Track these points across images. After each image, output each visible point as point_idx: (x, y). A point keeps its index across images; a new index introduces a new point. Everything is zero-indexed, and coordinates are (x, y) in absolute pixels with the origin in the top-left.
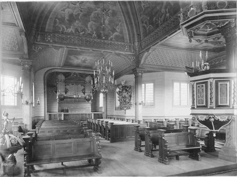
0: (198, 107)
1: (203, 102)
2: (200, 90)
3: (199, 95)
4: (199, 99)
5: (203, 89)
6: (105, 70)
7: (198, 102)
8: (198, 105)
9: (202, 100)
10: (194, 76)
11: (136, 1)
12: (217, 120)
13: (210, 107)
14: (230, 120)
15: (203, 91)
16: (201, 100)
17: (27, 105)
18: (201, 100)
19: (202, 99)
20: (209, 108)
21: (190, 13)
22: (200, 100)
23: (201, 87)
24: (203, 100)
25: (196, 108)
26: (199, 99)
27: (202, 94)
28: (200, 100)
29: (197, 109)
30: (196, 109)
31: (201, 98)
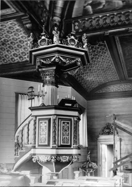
0: (39, 146)
2: (43, 127)
5: (69, 127)
6: (130, 36)
7: (63, 140)
8: (39, 144)
9: (67, 138)
10: (17, 118)
11: (33, 1)
12: (59, 160)
13: (52, 146)
14: (71, 161)
15: (68, 129)
16: (66, 138)
17: (116, 176)
18: (66, 138)
19: (68, 138)
20: (51, 147)
21: (64, 18)
22: (65, 138)
23: (66, 124)
25: (37, 147)
26: (41, 137)
28: (65, 138)
29: (59, 149)
30: (38, 148)
31: (66, 136)
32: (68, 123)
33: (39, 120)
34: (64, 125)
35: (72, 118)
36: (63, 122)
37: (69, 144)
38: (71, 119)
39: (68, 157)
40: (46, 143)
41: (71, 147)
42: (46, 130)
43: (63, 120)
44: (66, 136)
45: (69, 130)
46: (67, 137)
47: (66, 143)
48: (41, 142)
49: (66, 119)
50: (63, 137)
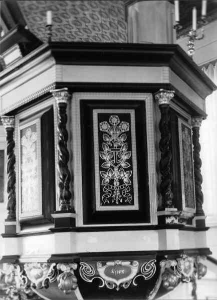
1: (132, 192)
3: (107, 158)
4: (107, 177)
5: (128, 134)
7: (102, 193)
9: (121, 181)
15: (128, 141)
16: (117, 183)
18: (117, 183)
20: (154, 222)
22: (112, 181)
23: (115, 120)
24: (132, 186)
25: (80, 223)
27: (125, 157)
28: (112, 181)
31: (116, 174)
32: (125, 118)
33: (86, 108)
34: (105, 126)
35: (147, 98)
36: (99, 115)
37: (136, 207)
38: (143, 103)
39: (136, 263)
40: (132, 204)
41: (147, 220)
42: (130, 149)
43: (127, 106)
44: (116, 174)
45: (130, 149)
46: (125, 177)
47: (120, 204)
48: (111, 199)
49: (127, 104)
50: (101, 179)
